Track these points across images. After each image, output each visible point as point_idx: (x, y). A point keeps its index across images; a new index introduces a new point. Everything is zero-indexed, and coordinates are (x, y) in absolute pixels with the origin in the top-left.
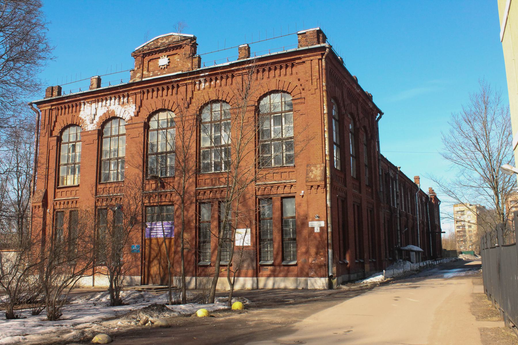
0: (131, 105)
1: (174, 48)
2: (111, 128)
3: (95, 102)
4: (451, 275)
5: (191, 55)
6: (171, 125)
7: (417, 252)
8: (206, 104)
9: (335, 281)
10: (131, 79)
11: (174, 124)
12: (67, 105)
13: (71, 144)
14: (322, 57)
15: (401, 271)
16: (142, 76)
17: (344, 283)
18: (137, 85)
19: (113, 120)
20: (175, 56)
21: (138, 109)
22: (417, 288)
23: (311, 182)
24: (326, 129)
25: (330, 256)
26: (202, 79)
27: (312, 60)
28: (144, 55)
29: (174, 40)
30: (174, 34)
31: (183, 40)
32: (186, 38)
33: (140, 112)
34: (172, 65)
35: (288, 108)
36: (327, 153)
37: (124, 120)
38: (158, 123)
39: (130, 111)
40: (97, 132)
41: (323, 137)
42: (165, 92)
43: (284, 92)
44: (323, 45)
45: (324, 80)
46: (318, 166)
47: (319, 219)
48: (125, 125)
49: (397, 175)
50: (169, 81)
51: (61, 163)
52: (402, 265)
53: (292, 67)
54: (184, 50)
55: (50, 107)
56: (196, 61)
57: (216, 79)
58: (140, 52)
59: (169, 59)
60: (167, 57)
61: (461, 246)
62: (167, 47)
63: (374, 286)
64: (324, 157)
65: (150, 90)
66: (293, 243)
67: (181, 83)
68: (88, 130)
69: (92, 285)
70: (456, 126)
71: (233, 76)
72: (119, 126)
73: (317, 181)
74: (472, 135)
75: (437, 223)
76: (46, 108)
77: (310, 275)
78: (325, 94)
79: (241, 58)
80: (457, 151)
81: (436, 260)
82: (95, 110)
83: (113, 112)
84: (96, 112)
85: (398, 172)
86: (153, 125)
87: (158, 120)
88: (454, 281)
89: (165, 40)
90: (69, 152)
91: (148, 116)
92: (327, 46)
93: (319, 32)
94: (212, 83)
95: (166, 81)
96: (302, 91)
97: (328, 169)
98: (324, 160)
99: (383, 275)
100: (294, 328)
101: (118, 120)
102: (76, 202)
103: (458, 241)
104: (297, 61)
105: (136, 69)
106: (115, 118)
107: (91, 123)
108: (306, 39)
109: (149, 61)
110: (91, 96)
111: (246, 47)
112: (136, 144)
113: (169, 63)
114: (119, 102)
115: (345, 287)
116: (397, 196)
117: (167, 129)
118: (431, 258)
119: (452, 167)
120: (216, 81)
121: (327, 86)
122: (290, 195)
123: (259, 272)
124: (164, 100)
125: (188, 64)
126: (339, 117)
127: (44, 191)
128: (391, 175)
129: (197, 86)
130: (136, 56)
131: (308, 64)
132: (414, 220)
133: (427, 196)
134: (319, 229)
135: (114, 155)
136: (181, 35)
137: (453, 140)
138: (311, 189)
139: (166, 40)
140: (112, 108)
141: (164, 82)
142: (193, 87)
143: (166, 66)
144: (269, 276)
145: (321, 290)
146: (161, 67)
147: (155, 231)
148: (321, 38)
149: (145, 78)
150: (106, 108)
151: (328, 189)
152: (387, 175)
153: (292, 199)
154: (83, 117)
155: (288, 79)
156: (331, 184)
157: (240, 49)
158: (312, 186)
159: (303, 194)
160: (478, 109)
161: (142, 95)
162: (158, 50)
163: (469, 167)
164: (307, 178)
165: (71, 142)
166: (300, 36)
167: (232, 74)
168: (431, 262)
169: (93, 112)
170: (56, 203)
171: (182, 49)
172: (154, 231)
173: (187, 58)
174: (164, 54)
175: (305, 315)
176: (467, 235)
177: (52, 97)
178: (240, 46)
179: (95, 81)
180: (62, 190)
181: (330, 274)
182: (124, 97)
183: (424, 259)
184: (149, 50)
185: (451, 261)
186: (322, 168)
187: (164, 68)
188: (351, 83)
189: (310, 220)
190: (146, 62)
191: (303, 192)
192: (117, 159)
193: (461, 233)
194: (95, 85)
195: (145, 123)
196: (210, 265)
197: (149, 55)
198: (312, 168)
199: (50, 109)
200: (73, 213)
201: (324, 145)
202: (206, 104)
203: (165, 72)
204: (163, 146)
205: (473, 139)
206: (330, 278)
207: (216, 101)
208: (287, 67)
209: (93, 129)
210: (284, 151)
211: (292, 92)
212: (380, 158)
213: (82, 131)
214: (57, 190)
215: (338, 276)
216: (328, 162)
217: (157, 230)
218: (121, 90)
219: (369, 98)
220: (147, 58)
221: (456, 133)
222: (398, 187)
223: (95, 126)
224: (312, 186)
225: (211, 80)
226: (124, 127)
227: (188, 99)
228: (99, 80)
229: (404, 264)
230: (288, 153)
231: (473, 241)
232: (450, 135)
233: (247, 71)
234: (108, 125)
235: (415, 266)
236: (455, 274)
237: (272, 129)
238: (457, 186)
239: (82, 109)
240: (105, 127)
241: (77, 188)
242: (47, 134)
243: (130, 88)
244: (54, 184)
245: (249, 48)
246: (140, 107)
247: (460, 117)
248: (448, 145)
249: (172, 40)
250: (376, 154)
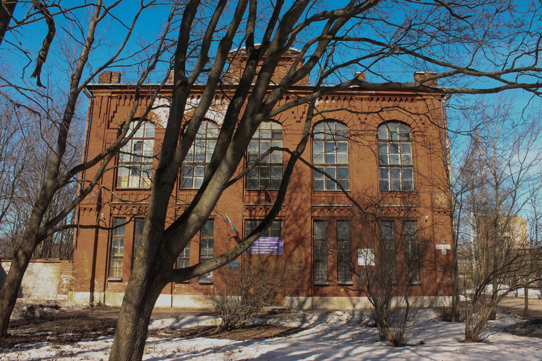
55: (110, 94)
69: (170, 306)
76: (104, 95)
147: (258, 247)
161: (118, 101)
172: (256, 247)
177: (111, 83)
178: (357, 72)
199: (109, 97)
210: (389, 181)
217: (259, 246)
233: (368, 96)
242: (103, 125)
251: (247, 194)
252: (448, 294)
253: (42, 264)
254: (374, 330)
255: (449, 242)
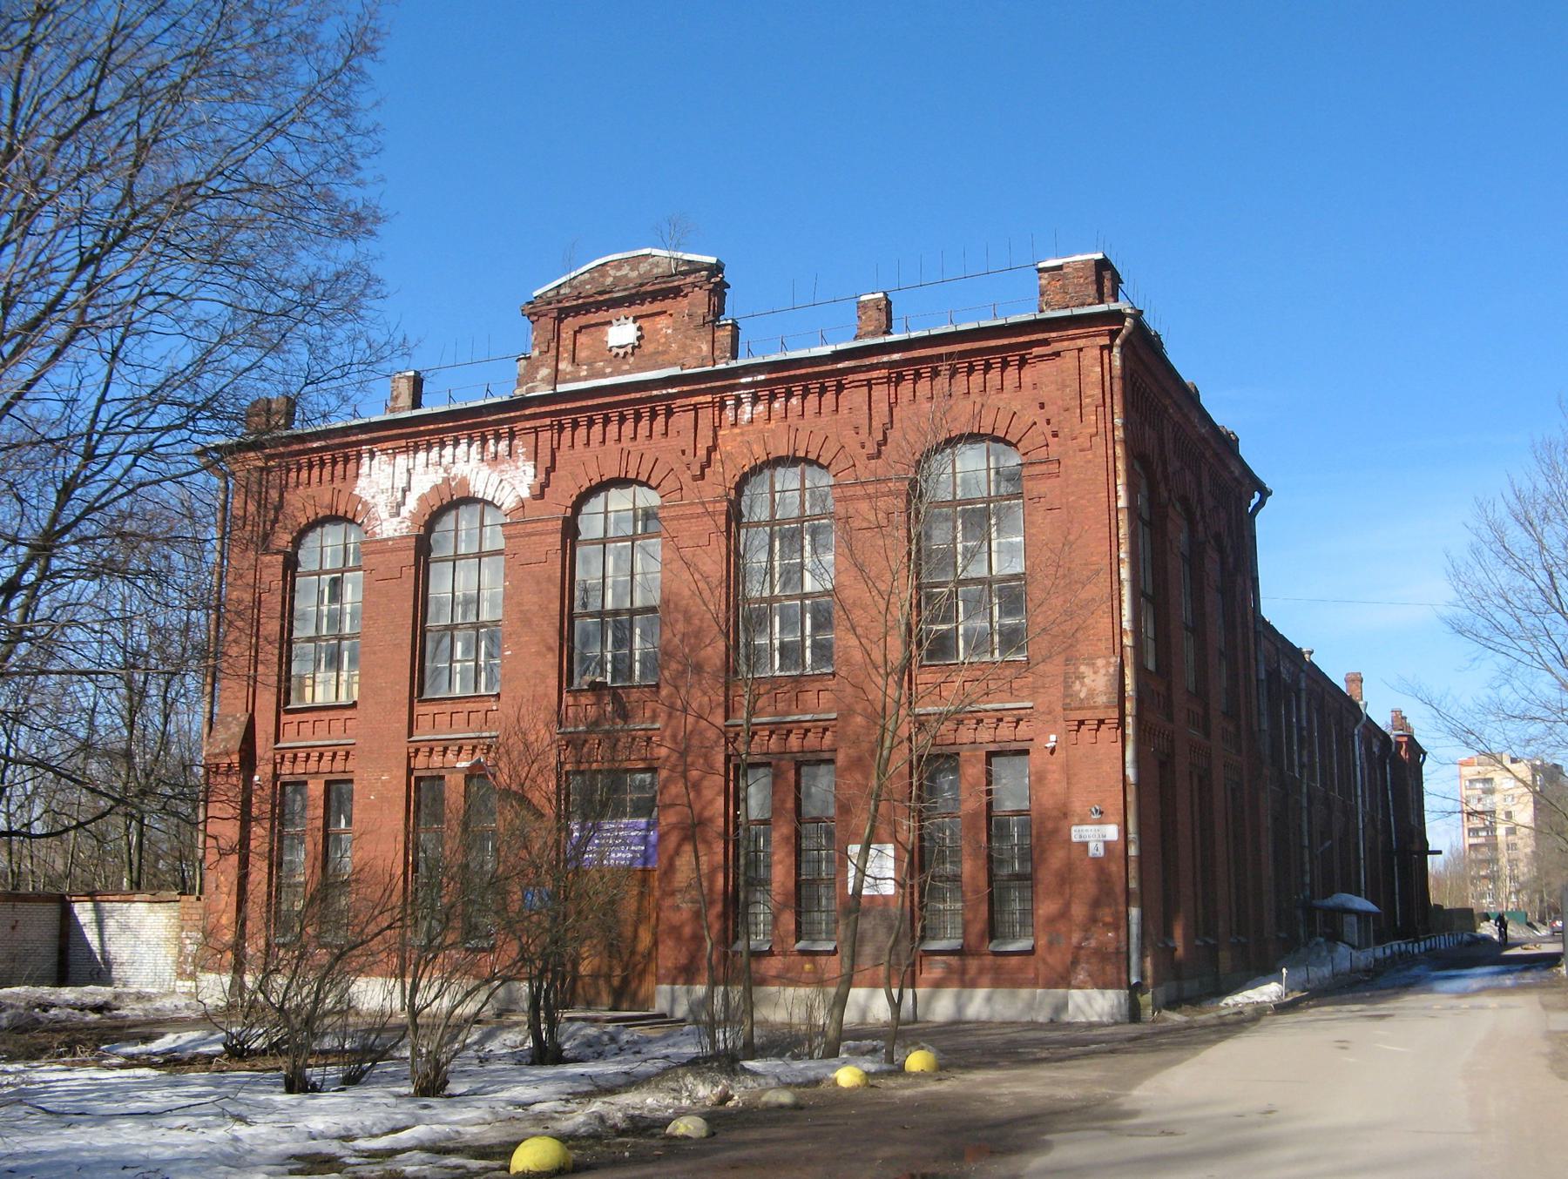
0: (520, 464)
1: (655, 296)
2: (457, 530)
3: (406, 450)
4: (1474, 984)
5: (711, 318)
6: (645, 527)
7: (1362, 915)
8: (756, 470)
9: (1145, 999)
10: (519, 385)
11: (652, 526)
12: (315, 458)
13: (327, 578)
14: (1112, 340)
15: (1326, 971)
16: (556, 378)
17: (1172, 1005)
18: (540, 406)
19: (462, 508)
20: (658, 319)
21: (542, 477)
22: (1387, 1019)
23: (1079, 709)
24: (1122, 555)
25: (1134, 929)
26: (744, 394)
27: (1080, 350)
28: (563, 314)
29: (656, 271)
30: (655, 252)
31: (685, 274)
32: (695, 268)
33: (548, 485)
34: (649, 348)
35: (1005, 488)
36: (1126, 625)
37: (499, 508)
38: (606, 518)
39: (516, 483)
40: (412, 543)
41: (1115, 578)
42: (628, 427)
43: (997, 440)
44: (1114, 306)
45: (1117, 409)
46: (1100, 662)
47: (1102, 817)
48: (502, 525)
49: (1302, 675)
50: (644, 394)
51: (296, 634)
52: (1324, 954)
53: (1020, 368)
54: (686, 301)
56: (724, 335)
57: (789, 395)
58: (549, 303)
59: (640, 329)
60: (634, 322)
61: (1482, 896)
62: (633, 291)
63: (1258, 1014)
64: (1117, 638)
65: (583, 420)
66: (1020, 888)
67: (679, 402)
68: (385, 536)
70: (1488, 535)
71: (840, 388)
72: (482, 525)
73: (1096, 708)
74: (1538, 565)
75: (1414, 821)
77: (1073, 982)
78: (1119, 450)
79: (866, 335)
80: (1493, 609)
81: (1417, 941)
82: (405, 475)
83: (464, 482)
84: (409, 482)
85: (1305, 668)
86: (591, 525)
87: (606, 512)
88: (1491, 1001)
89: (625, 270)
90: (320, 602)
91: (574, 498)
92: (1129, 311)
93: (1103, 266)
94: (776, 405)
95: (633, 396)
96: (1051, 440)
97: (1128, 672)
98: (1118, 647)
99: (1280, 982)
100: (1127, 1107)
101: (479, 507)
102: (347, 754)
103: (1473, 878)
104: (1036, 351)
105: (536, 353)
106: (470, 500)
107: (392, 516)
108: (1063, 286)
109: (575, 332)
110: (395, 432)
111: (879, 299)
112: (538, 583)
113: (639, 339)
114: (482, 453)
115: (1176, 1017)
116: (1301, 739)
117: (633, 539)
118: (1400, 935)
119: (1475, 659)
120: (787, 401)
121: (1125, 426)
122: (1014, 746)
123: (918, 972)
124: (626, 452)
125: (699, 343)
126: (1151, 514)
127: (244, 718)
128: (1285, 675)
129: (729, 413)
130: (535, 314)
131: (1069, 360)
132: (1349, 813)
133: (1386, 736)
134: (1101, 846)
135: (465, 615)
136: (679, 255)
137: (1481, 575)
138: (1078, 731)
139: (632, 270)
140: (460, 469)
141: (627, 397)
142: (717, 416)
143: (629, 349)
144: (938, 984)
145: (1107, 1026)
146: (615, 351)
148: (1107, 284)
149: (565, 381)
150: (441, 470)
151: (1130, 731)
152: (1273, 674)
153: (1017, 760)
154: (366, 497)
155: (1009, 401)
156: (1139, 718)
157: (863, 306)
158: (1081, 723)
159: (1053, 744)
160: (1555, 486)
161: (556, 436)
162: (605, 300)
163: (1527, 659)
164: (1066, 696)
165: (327, 572)
166: (1046, 275)
167: (839, 382)
168: (1403, 947)
169: (401, 482)
170: (283, 757)
171: (679, 299)
173: (696, 327)
174: (624, 311)
175: (1141, 1075)
176: (1503, 861)
178: (863, 298)
179: (405, 389)
180: (300, 717)
181: (1134, 980)
182: (498, 438)
183: (1380, 939)
184: (578, 298)
185: (1460, 943)
186: (1111, 670)
187: (626, 353)
188: (1186, 410)
189: (1076, 820)
190: (566, 335)
191: (1053, 737)
192: (477, 626)
193: (1484, 855)
194: (405, 399)
195: (565, 520)
196: (770, 953)
197: (577, 314)
198: (1083, 668)
200: (334, 787)
201: (1116, 603)
202: (756, 470)
203: (626, 367)
204: (620, 589)
205: (1542, 577)
206: (1135, 990)
207: (791, 461)
208: (1005, 364)
209: (397, 534)
211: (1020, 440)
212: (1260, 628)
213: (364, 537)
214: (284, 718)
215: (1156, 984)
216: (1129, 652)
218: (489, 419)
219: (1227, 444)
220: (570, 324)
221: (1488, 555)
222: (1304, 713)
223: (404, 525)
224: (1081, 723)
225: (773, 397)
226: (499, 528)
227: (702, 453)
228: (417, 383)
229: (1330, 951)
230: (1008, 621)
231: (1521, 879)
232: (1470, 560)
233: (884, 372)
234: (448, 521)
235: (1364, 958)
236: (1486, 982)
237: (960, 547)
238: (1492, 718)
239: (364, 470)
240: (438, 528)
241: (348, 713)
243: (518, 413)
244: (274, 699)
245: (889, 303)
246: (551, 469)
247: (1502, 509)
248: (1466, 592)
249: (650, 270)
250: (1250, 617)
251: (571, 700)
252: (1100, 984)
253: (146, 905)
254: (203, 1042)
255: (1112, 818)
